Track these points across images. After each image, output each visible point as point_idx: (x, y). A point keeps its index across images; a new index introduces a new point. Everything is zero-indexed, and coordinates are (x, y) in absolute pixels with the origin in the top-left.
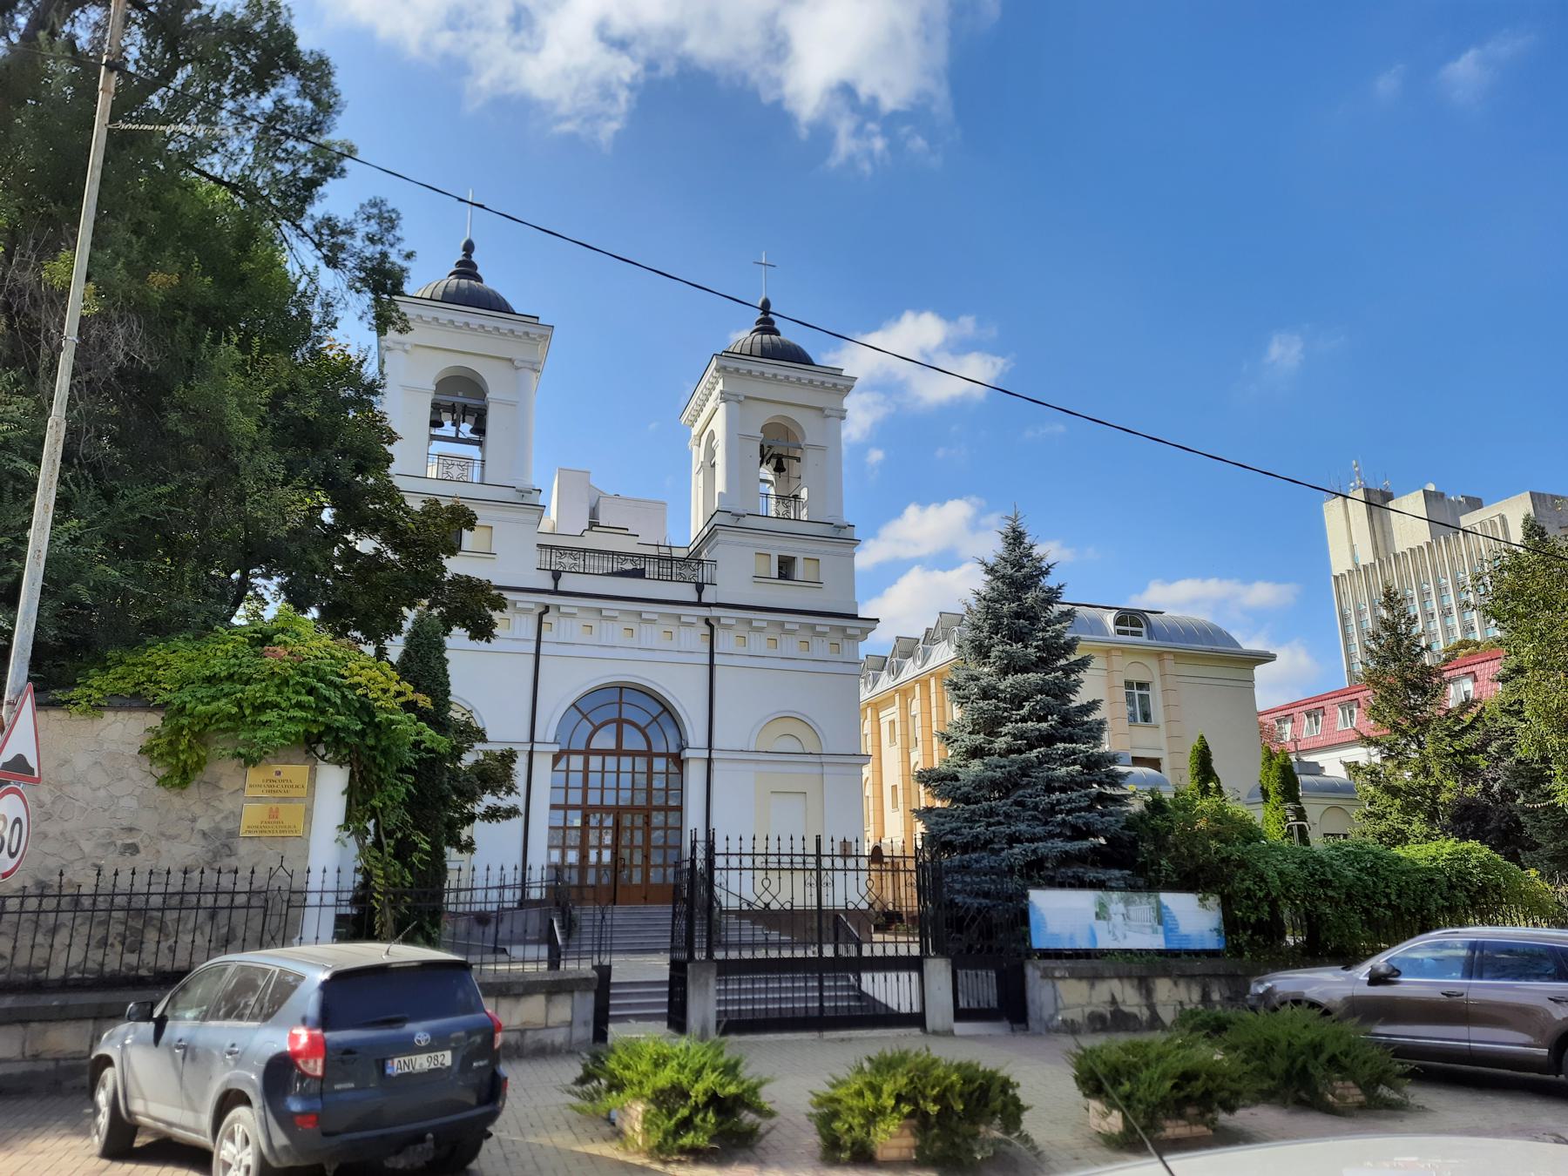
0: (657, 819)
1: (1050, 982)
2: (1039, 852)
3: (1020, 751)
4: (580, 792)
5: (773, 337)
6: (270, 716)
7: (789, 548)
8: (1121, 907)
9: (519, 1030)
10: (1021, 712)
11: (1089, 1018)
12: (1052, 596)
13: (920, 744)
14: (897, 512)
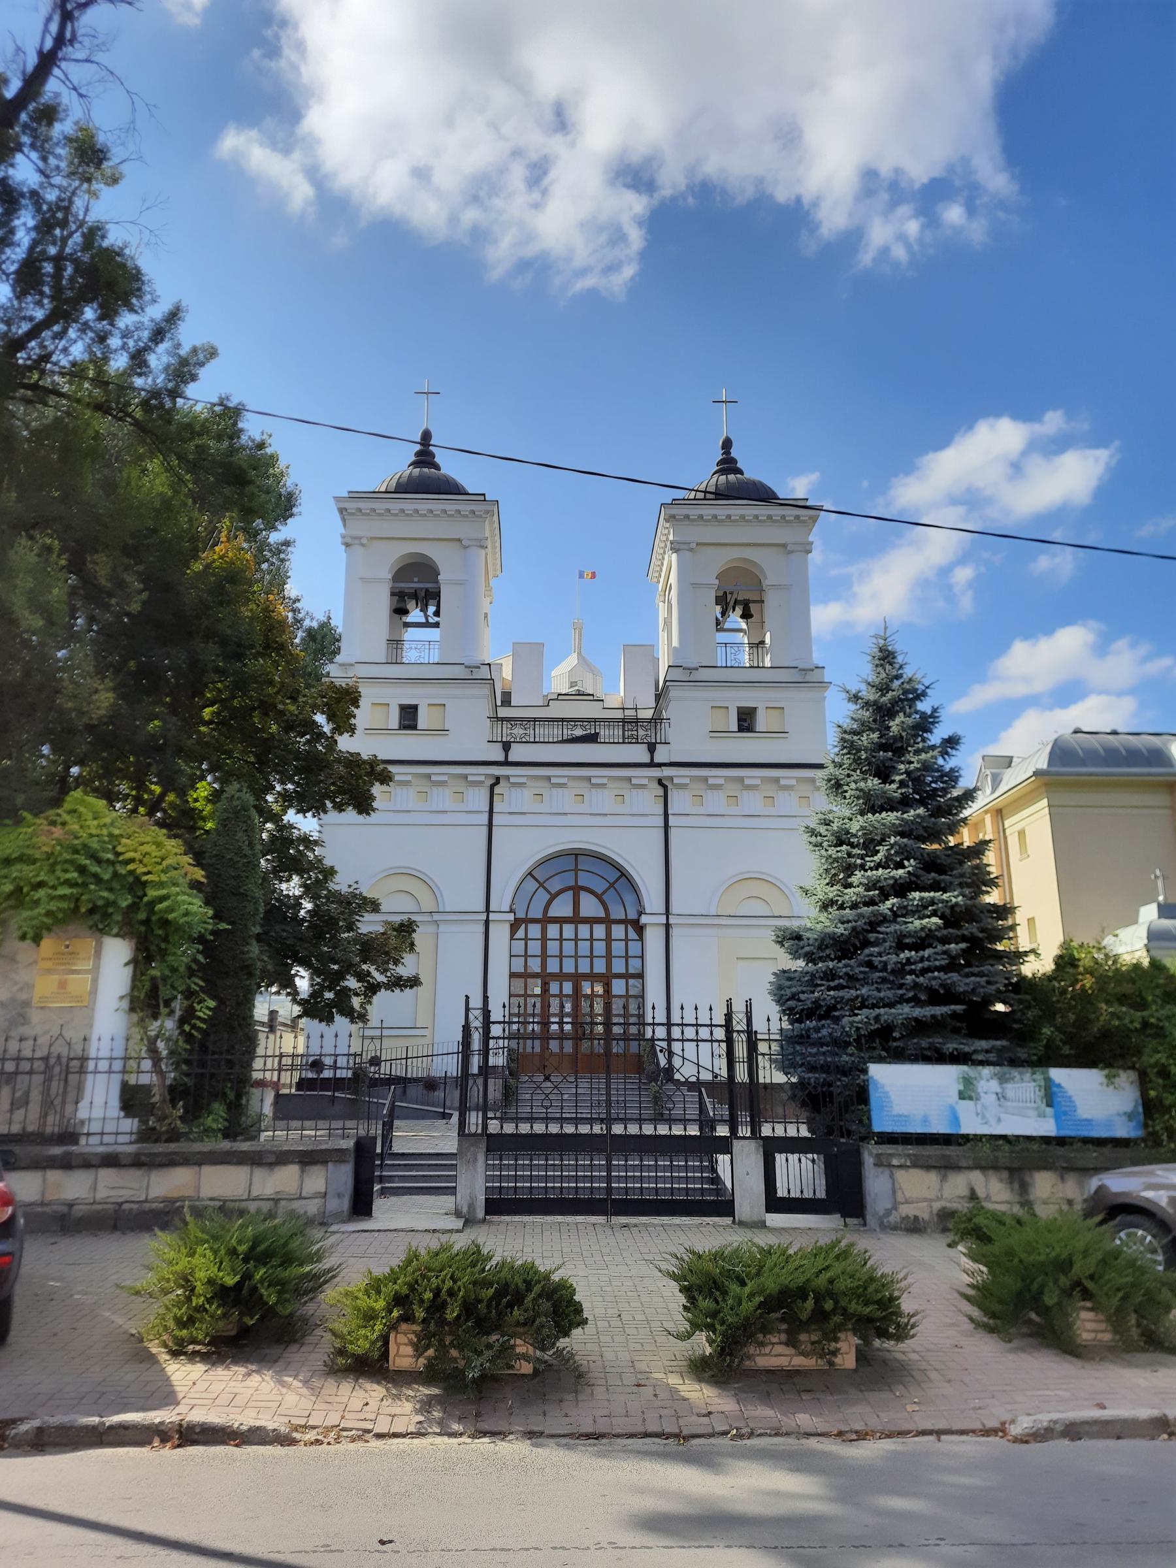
0: (618, 987)
1: (887, 1171)
2: (882, 1019)
3: (871, 902)
5: (739, 476)
6: (41, 893)
7: (747, 699)
8: (994, 1085)
9: (273, 1199)
10: (875, 858)
11: (938, 1215)
12: (926, 723)
14: (1003, 648)
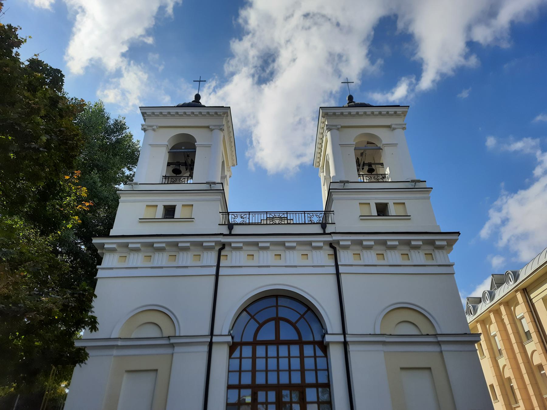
4: (250, 374)
7: (382, 198)
13: (504, 352)
